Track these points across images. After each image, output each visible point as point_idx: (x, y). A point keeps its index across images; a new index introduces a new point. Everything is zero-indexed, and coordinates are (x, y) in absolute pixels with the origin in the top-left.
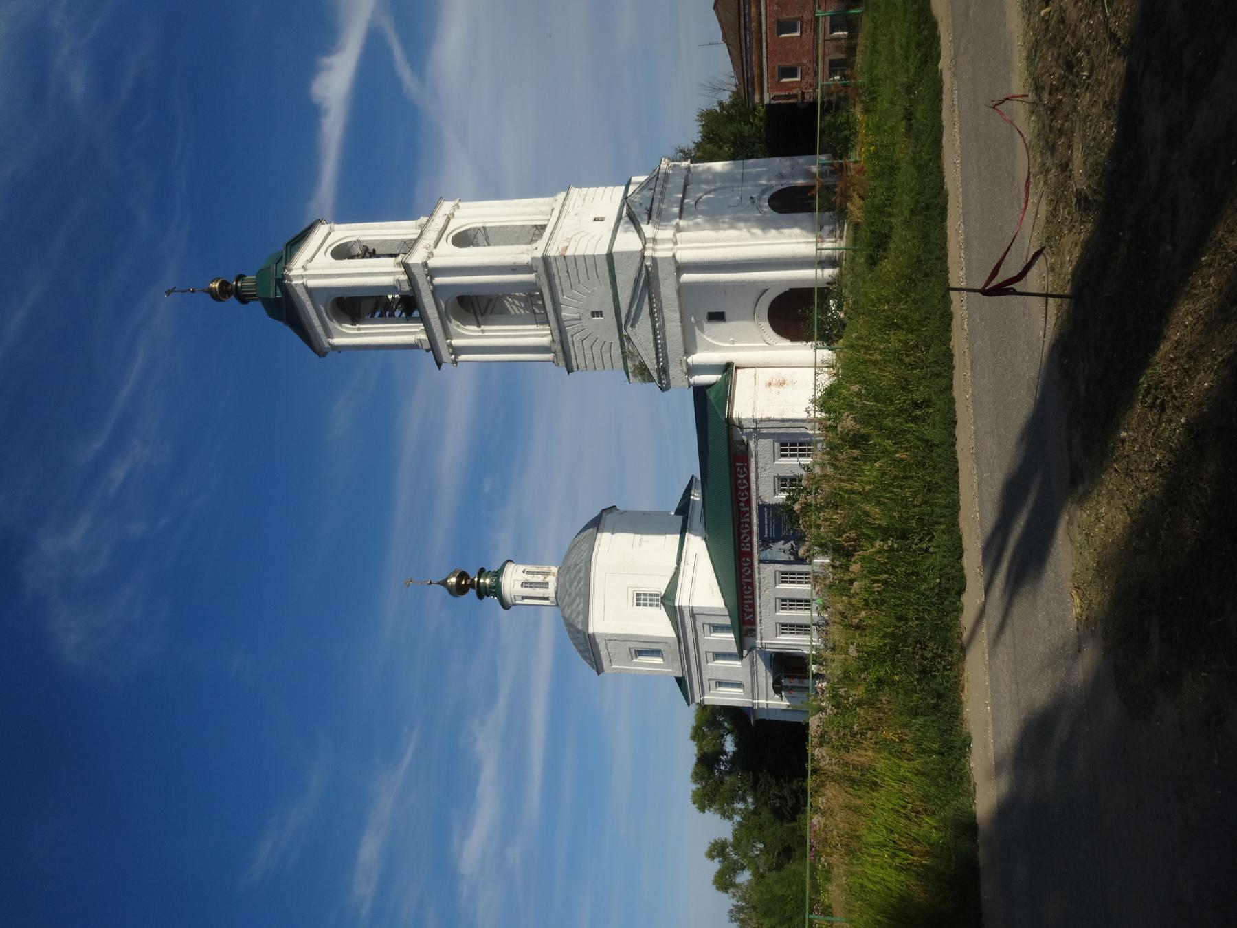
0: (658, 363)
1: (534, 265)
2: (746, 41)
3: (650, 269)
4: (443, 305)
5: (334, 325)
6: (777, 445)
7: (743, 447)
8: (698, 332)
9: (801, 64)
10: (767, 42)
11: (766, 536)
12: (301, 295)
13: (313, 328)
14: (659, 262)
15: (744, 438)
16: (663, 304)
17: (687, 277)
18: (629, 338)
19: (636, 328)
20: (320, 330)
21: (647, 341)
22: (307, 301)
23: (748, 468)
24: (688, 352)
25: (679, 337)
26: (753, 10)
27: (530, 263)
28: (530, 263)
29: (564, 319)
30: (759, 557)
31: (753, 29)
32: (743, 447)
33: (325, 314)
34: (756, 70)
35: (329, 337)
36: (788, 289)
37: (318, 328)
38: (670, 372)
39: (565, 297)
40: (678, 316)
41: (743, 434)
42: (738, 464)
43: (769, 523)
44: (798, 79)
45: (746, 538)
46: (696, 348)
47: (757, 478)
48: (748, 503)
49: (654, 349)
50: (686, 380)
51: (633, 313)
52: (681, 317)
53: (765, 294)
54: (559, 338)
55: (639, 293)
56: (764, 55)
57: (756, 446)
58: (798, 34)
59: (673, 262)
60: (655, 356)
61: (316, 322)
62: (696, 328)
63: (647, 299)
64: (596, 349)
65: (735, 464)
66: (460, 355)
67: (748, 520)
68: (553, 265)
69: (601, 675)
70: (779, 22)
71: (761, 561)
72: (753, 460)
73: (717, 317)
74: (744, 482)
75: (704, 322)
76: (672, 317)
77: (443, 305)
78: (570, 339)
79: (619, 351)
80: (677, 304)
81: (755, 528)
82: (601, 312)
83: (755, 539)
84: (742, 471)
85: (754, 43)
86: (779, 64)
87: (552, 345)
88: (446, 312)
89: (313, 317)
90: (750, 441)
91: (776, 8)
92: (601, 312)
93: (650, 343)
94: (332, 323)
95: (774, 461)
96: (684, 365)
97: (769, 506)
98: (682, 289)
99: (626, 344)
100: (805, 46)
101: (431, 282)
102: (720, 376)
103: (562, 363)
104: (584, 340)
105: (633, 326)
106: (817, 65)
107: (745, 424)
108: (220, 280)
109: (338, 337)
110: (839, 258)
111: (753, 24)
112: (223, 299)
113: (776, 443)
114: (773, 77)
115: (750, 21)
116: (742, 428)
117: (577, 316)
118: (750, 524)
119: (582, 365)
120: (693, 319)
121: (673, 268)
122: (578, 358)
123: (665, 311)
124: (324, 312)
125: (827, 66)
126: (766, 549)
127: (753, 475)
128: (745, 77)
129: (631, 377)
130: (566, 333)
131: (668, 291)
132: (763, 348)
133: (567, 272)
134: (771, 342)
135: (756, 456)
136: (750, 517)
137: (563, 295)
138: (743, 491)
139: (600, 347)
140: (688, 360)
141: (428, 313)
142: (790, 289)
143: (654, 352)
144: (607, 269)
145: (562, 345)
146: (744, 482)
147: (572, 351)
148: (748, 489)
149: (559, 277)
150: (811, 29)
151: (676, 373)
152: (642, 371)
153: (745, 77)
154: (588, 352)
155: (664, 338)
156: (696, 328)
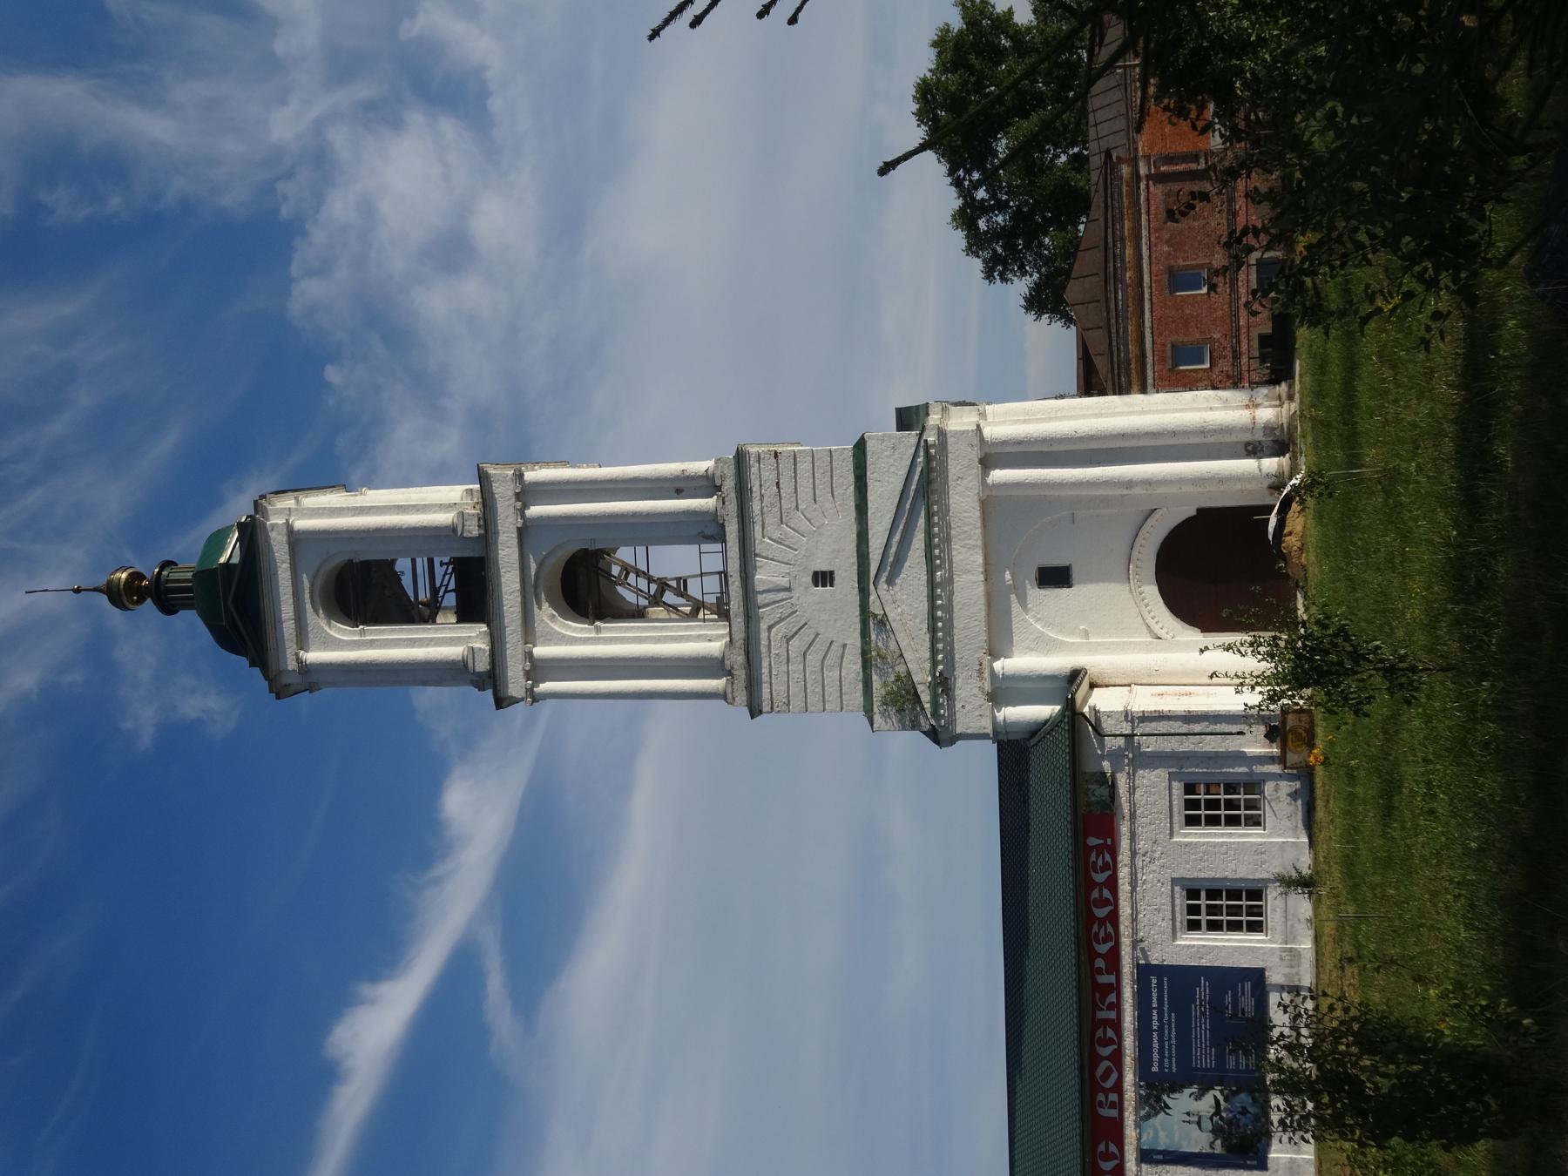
0: (934, 663)
1: (718, 473)
2: (1116, 298)
3: (933, 451)
4: (533, 566)
5: (318, 622)
6: (1178, 787)
7: (1103, 792)
8: (1016, 607)
9: (1211, 341)
10: (1152, 303)
11: (1155, 1069)
12: (275, 549)
13: (278, 622)
14: (950, 440)
15: (1106, 765)
16: (953, 532)
17: (998, 475)
18: (883, 622)
19: (897, 588)
20: (289, 628)
21: (916, 617)
22: (283, 562)
23: (1113, 851)
24: (994, 654)
25: (979, 609)
26: (1129, 251)
27: (710, 472)
28: (710, 472)
29: (759, 588)
30: (1139, 1139)
31: (1128, 281)
32: (1103, 792)
33: (307, 596)
34: (1133, 348)
35: (302, 649)
36: (1193, 513)
37: (285, 625)
38: (957, 692)
39: (766, 540)
40: (980, 559)
41: (1102, 757)
42: (1092, 841)
43: (1161, 1028)
44: (1207, 366)
45: (1108, 1072)
46: (1012, 642)
47: (1133, 884)
48: (1114, 958)
49: (928, 636)
50: (988, 713)
51: (893, 550)
52: (986, 563)
53: (1151, 521)
54: (743, 635)
55: (908, 506)
56: (1148, 323)
57: (1132, 790)
58: (1207, 366)
59: (976, 442)
60: (928, 655)
61: (287, 610)
62: (1013, 597)
63: (922, 522)
64: (814, 658)
65: (1085, 843)
66: (544, 682)
67: (1112, 1015)
68: (752, 469)
69: (755, 719)
70: (1171, 271)
71: (1146, 1156)
72: (1124, 829)
73: (1055, 577)
74: (1106, 894)
75: (1028, 586)
76: (967, 558)
77: (533, 566)
78: (764, 635)
79: (858, 667)
80: (978, 531)
81: (1129, 1042)
82: (832, 573)
83: (1129, 1077)
84: (1102, 934)
85: (1131, 304)
86: (1173, 338)
87: (727, 653)
88: (536, 586)
89: (283, 598)
90: (1118, 775)
91: (1166, 248)
92: (832, 573)
93: (921, 622)
94: (316, 616)
95: (1171, 835)
96: (986, 675)
97: (1162, 970)
98: (992, 504)
99: (873, 637)
100: (1216, 310)
101: (522, 512)
102: (1058, 708)
103: (741, 696)
104: (793, 636)
105: (890, 582)
106: (1239, 342)
107: (1108, 725)
108: (130, 571)
109: (319, 649)
110: (1289, 425)
111: (1128, 274)
112: (131, 606)
113: (1175, 784)
114: (1163, 360)
115: (1124, 269)
116: (1099, 733)
117: (784, 582)
118: (1117, 1026)
119: (780, 698)
120: (1008, 576)
121: (975, 455)
122: (774, 685)
123: (955, 546)
124: (307, 591)
125: (1255, 344)
126: (1156, 1114)
127: (1124, 873)
128: (1115, 359)
129: (877, 718)
130: (758, 620)
131: (962, 501)
132: (1147, 648)
133: (778, 484)
134: (1162, 633)
135: (1133, 816)
136: (1117, 1006)
137: (763, 537)
138: (1102, 921)
139: (820, 657)
140: (994, 664)
141: (503, 580)
142: (1203, 513)
143: (927, 644)
144: (851, 478)
145: (747, 653)
146: (1106, 894)
147: (765, 664)
148: (1114, 918)
149: (762, 496)
150: (1225, 283)
151: (971, 709)
152: (904, 701)
153: (1115, 359)
154: (796, 667)
155: (949, 608)
156: (1013, 597)
